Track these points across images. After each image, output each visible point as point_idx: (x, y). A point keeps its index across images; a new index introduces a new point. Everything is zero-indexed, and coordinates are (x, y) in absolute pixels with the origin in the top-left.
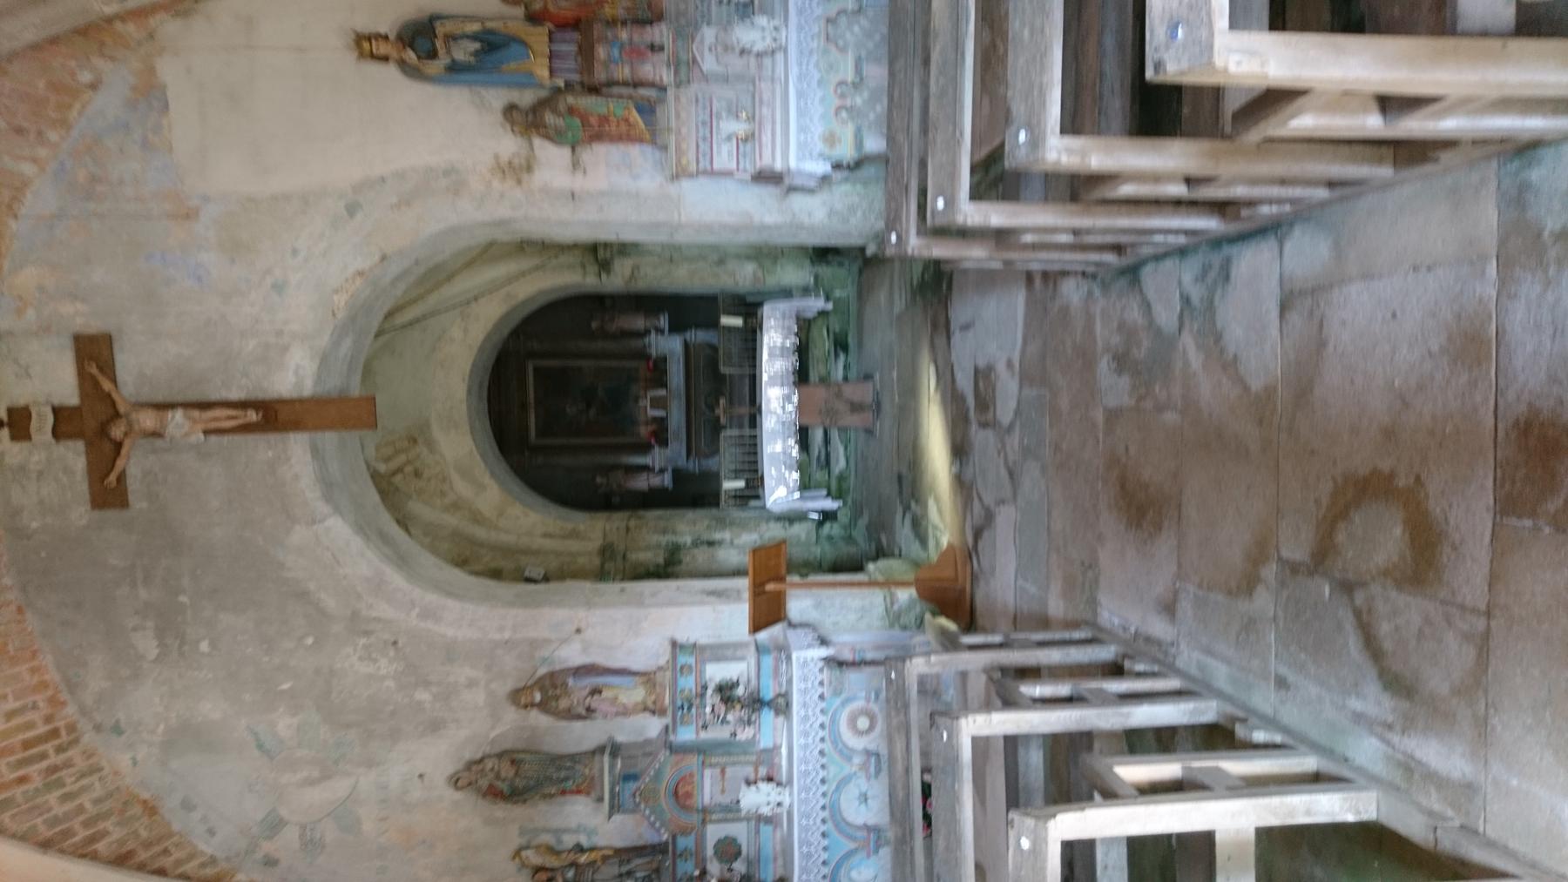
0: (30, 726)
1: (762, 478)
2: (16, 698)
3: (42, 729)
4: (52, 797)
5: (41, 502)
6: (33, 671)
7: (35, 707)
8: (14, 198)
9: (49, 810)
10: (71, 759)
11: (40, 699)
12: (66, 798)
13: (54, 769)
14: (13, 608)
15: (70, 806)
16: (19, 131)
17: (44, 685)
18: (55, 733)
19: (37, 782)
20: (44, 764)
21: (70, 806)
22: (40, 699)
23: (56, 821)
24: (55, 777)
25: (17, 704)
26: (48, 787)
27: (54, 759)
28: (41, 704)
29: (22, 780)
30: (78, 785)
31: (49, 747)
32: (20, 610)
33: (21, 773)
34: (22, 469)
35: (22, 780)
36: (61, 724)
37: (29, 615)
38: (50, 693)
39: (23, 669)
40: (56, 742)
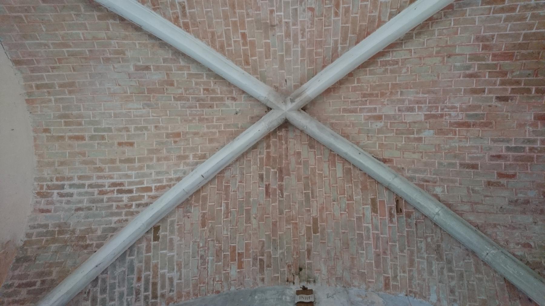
0: (163, 287)
1: (214, 153)
2: (178, 284)
3: (159, 292)
4: (125, 289)
5: (266, 299)
6: (188, 293)
7: (171, 291)
8: (415, 293)
9: (119, 287)
10: (138, 268)
11: (174, 294)
12: (121, 295)
13: (138, 293)
14: (220, 289)
15: (117, 295)
16: (452, 291)
17: (180, 296)
18: (155, 297)
19: (135, 285)
20: (142, 289)
21: (117, 295)
22: (174, 294)
23: (113, 287)
24: (134, 293)
25: (175, 284)
26: (130, 289)
27: (142, 295)
28: (171, 294)
29: (139, 279)
30: (125, 301)
31: (150, 293)
32: (218, 292)
33: (143, 279)
34: (283, 294)
35: (139, 279)
36: (158, 300)
37: (214, 295)
38: (175, 298)
39: (191, 289)
40: (150, 297)
